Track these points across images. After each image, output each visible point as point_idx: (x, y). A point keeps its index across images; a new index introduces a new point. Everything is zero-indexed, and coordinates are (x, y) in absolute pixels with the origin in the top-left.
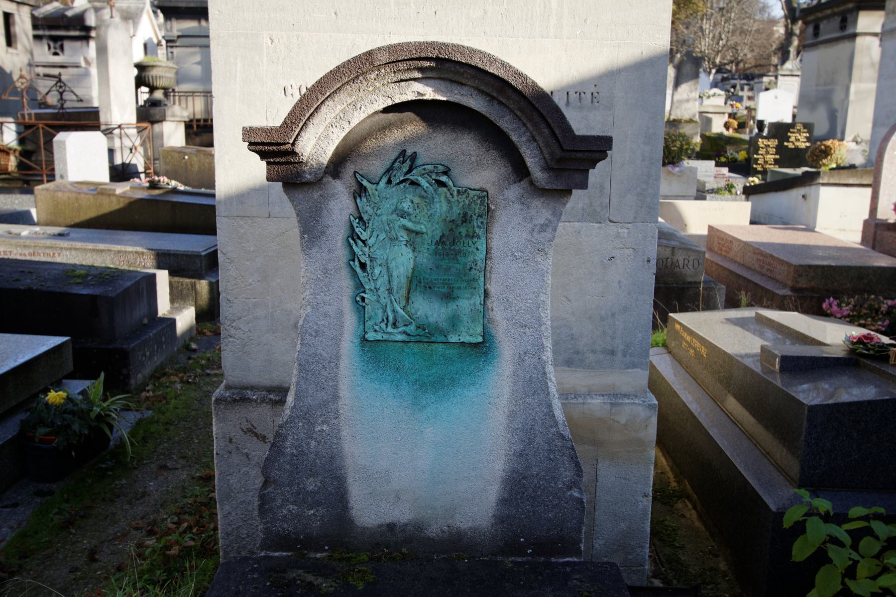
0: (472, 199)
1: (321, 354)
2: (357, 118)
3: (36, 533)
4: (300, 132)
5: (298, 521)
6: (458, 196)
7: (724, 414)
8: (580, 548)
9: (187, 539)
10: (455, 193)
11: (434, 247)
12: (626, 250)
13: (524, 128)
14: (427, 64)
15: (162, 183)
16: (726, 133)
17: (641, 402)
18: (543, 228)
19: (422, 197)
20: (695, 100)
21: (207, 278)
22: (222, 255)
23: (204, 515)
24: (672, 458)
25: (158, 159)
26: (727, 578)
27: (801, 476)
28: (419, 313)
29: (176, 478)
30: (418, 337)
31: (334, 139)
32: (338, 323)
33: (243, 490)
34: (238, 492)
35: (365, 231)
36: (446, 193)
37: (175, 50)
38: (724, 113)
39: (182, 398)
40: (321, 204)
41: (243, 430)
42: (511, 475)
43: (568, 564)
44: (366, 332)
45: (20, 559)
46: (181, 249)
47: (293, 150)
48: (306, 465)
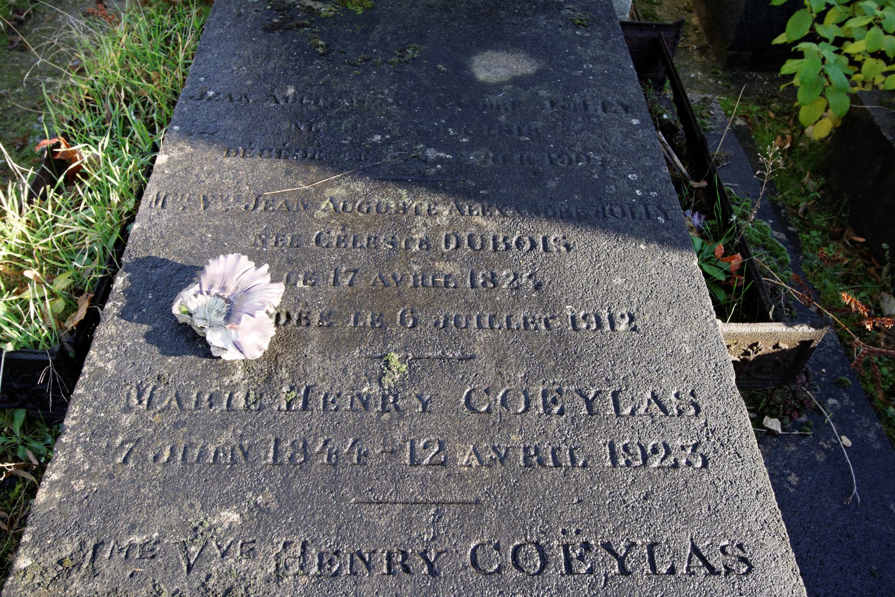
26: (697, 32)
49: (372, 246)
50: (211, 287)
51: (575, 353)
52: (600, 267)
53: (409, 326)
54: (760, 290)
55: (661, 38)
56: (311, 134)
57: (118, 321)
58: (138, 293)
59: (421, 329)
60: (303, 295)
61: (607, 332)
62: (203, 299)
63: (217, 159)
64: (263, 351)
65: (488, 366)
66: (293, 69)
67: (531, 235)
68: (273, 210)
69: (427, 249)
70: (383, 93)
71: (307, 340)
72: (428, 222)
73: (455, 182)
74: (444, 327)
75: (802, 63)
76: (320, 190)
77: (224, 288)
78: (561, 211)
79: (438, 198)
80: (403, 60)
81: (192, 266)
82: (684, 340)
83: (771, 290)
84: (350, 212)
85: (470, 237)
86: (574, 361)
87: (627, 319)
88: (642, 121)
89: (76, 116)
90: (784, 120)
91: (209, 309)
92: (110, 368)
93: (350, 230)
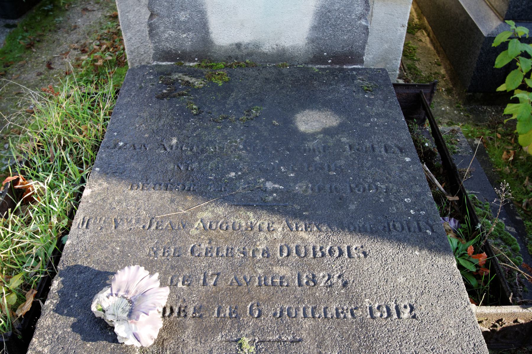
3: (11, 51)
5: (176, 42)
9: (107, 56)
23: (116, 40)
26: (445, 79)
27: (507, 13)
29: (94, 17)
33: (138, 23)
43: (354, 69)
45: (4, 67)
48: (178, 3)
49: (230, 255)
50: (119, 290)
51: (373, 336)
52: (388, 269)
53: (256, 316)
54: (501, 280)
55: (422, 94)
56: (188, 172)
57: (53, 314)
58: (68, 293)
59: (264, 319)
60: (182, 293)
61: (395, 319)
62: (113, 299)
63: (124, 191)
64: (154, 340)
65: (312, 347)
66: (176, 125)
67: (339, 245)
68: (162, 229)
69: (267, 257)
70: (236, 142)
71: (184, 328)
72: (268, 236)
73: (286, 206)
74: (280, 317)
75: (519, 106)
76: (193, 214)
77: (127, 292)
78: (359, 227)
79: (275, 219)
80: (249, 118)
81: (106, 272)
82: (450, 325)
83: (508, 273)
84: (214, 230)
85: (297, 247)
86: (372, 343)
87: (409, 309)
88: (413, 159)
89: (30, 158)
90: (508, 139)
91: (117, 307)
92: (46, 351)
93: (214, 243)
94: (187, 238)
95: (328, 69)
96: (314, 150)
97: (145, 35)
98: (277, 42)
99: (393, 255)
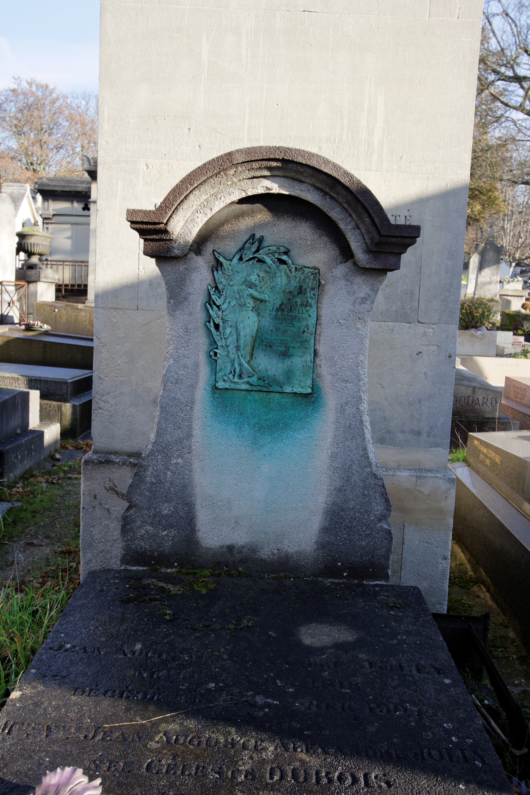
0: (307, 275)
1: (179, 399)
2: (218, 206)
4: (172, 214)
5: (154, 540)
6: (295, 272)
7: (515, 510)
8: (387, 573)
10: (293, 270)
11: (274, 313)
12: (431, 347)
13: (350, 219)
14: (274, 164)
15: (36, 326)
16: (523, 311)
17: (442, 476)
18: (363, 301)
19: (267, 272)
20: (497, 282)
21: (71, 401)
22: (97, 340)
24: (469, 552)
25: (31, 314)
26: (515, 644)
28: (260, 367)
30: (259, 387)
31: (198, 222)
32: (195, 373)
33: (103, 540)
34: (99, 542)
35: (219, 298)
36: (286, 269)
37: (50, 226)
38: (522, 296)
39: (47, 494)
40: (185, 276)
41: (106, 488)
42: (332, 507)
43: (377, 585)
44: (216, 382)
46: (50, 377)
47: (166, 228)
48: (163, 492)
69: (252, 780)
72: (255, 755)
78: (381, 752)
84: (181, 745)
85: (294, 770)
94: (143, 752)
95: (344, 583)
96: (322, 665)
97: (109, 557)
98: (279, 545)
99: (428, 786)
